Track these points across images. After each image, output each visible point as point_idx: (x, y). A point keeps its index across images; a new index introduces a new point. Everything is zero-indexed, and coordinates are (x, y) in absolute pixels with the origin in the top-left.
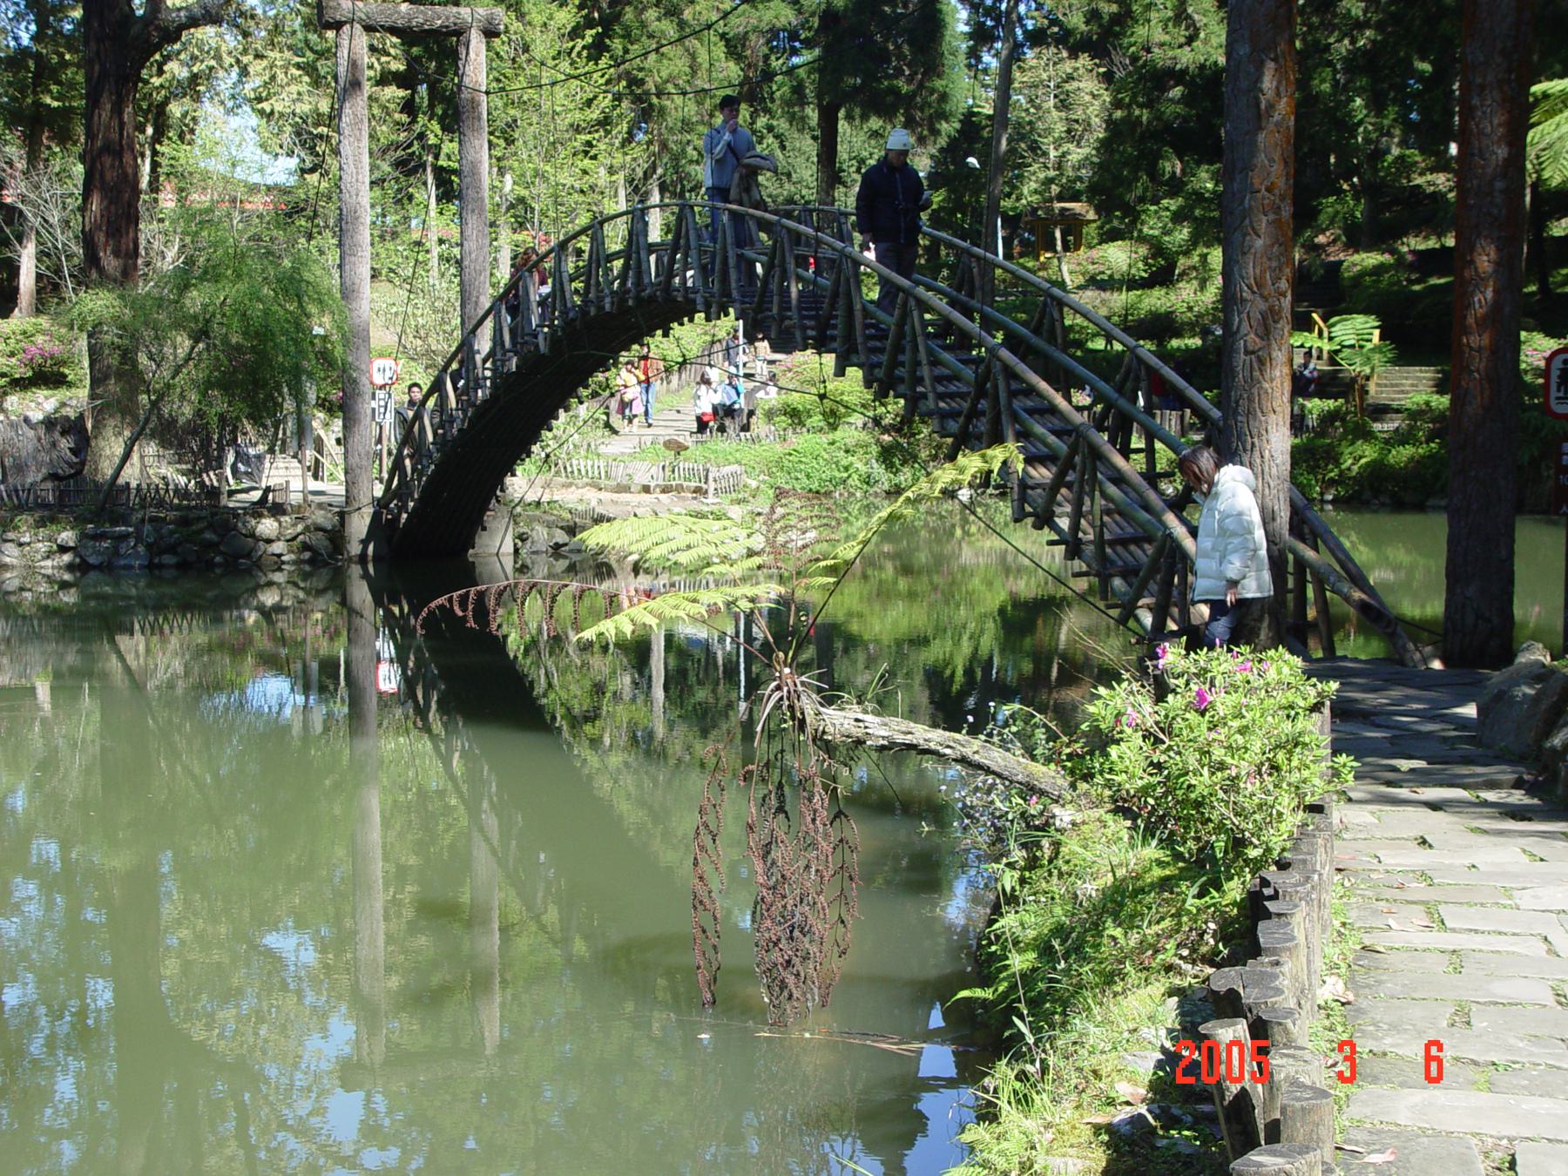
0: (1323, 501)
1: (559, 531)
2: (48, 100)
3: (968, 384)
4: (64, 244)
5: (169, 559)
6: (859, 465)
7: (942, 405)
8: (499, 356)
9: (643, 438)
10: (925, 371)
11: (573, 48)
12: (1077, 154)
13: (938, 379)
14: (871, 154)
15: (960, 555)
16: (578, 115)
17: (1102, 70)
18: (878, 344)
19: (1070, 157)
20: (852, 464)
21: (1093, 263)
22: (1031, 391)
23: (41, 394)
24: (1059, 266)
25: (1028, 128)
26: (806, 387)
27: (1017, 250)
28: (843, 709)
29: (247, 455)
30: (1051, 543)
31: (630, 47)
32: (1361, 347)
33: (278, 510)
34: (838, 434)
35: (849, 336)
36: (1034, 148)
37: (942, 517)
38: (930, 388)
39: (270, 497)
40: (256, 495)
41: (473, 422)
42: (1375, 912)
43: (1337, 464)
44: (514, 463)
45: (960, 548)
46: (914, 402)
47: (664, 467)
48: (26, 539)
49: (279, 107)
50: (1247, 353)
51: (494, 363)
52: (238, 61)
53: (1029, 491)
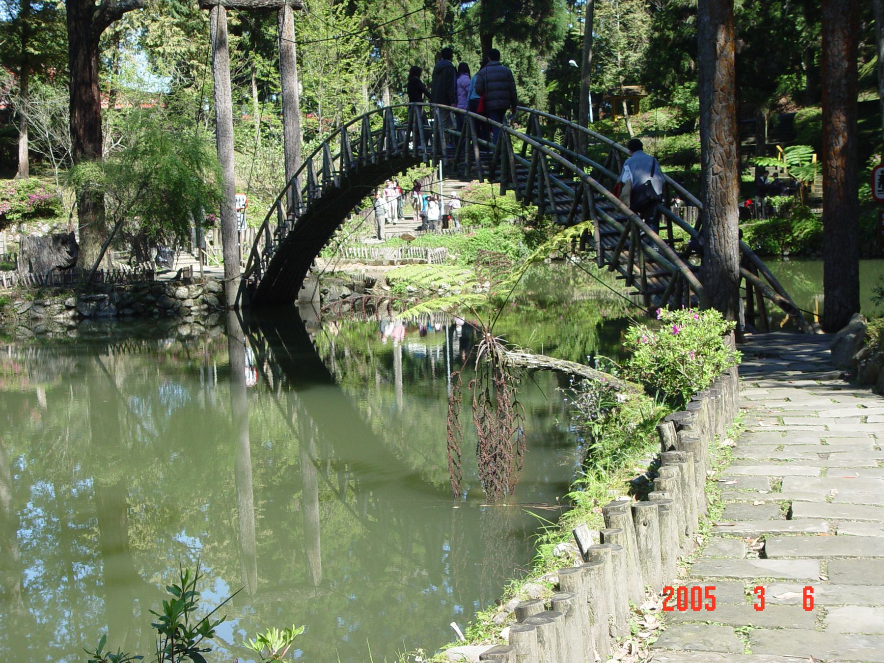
0: (783, 256)
1: (345, 288)
2: (32, 50)
3: (572, 196)
4: (50, 136)
5: (127, 311)
6: (513, 245)
7: (558, 208)
8: (311, 190)
9: (387, 235)
10: (548, 191)
11: (337, 9)
12: (634, 56)
13: (556, 195)
14: (512, 61)
15: (573, 296)
16: (341, 48)
17: (648, 6)
18: (523, 177)
19: (630, 59)
20: (508, 245)
21: (646, 121)
22: (605, 199)
23: (41, 222)
24: (626, 124)
25: (604, 43)
26: (480, 201)
27: (601, 115)
28: (516, 352)
29: (164, 252)
30: (618, 278)
31: (368, 5)
32: (803, 165)
33: (187, 282)
34: (500, 228)
35: (507, 174)
36: (610, 54)
37: (561, 273)
38: (551, 200)
39: (182, 275)
40: (172, 275)
41: (297, 227)
42: (755, 421)
43: (791, 234)
44: (320, 250)
45: (573, 291)
46: (543, 207)
47: (401, 250)
48: (48, 303)
49: (168, 50)
50: (714, 174)
51: (309, 193)
52: (142, 24)
53: (606, 252)
